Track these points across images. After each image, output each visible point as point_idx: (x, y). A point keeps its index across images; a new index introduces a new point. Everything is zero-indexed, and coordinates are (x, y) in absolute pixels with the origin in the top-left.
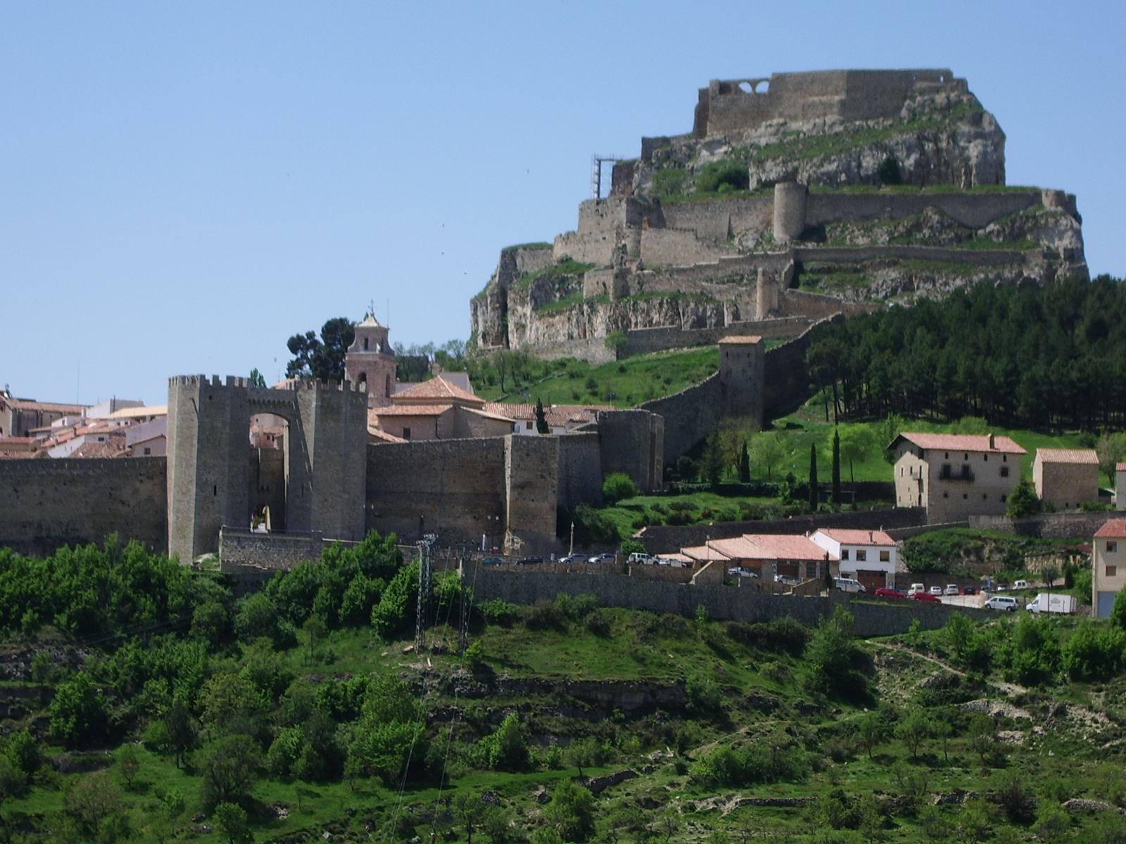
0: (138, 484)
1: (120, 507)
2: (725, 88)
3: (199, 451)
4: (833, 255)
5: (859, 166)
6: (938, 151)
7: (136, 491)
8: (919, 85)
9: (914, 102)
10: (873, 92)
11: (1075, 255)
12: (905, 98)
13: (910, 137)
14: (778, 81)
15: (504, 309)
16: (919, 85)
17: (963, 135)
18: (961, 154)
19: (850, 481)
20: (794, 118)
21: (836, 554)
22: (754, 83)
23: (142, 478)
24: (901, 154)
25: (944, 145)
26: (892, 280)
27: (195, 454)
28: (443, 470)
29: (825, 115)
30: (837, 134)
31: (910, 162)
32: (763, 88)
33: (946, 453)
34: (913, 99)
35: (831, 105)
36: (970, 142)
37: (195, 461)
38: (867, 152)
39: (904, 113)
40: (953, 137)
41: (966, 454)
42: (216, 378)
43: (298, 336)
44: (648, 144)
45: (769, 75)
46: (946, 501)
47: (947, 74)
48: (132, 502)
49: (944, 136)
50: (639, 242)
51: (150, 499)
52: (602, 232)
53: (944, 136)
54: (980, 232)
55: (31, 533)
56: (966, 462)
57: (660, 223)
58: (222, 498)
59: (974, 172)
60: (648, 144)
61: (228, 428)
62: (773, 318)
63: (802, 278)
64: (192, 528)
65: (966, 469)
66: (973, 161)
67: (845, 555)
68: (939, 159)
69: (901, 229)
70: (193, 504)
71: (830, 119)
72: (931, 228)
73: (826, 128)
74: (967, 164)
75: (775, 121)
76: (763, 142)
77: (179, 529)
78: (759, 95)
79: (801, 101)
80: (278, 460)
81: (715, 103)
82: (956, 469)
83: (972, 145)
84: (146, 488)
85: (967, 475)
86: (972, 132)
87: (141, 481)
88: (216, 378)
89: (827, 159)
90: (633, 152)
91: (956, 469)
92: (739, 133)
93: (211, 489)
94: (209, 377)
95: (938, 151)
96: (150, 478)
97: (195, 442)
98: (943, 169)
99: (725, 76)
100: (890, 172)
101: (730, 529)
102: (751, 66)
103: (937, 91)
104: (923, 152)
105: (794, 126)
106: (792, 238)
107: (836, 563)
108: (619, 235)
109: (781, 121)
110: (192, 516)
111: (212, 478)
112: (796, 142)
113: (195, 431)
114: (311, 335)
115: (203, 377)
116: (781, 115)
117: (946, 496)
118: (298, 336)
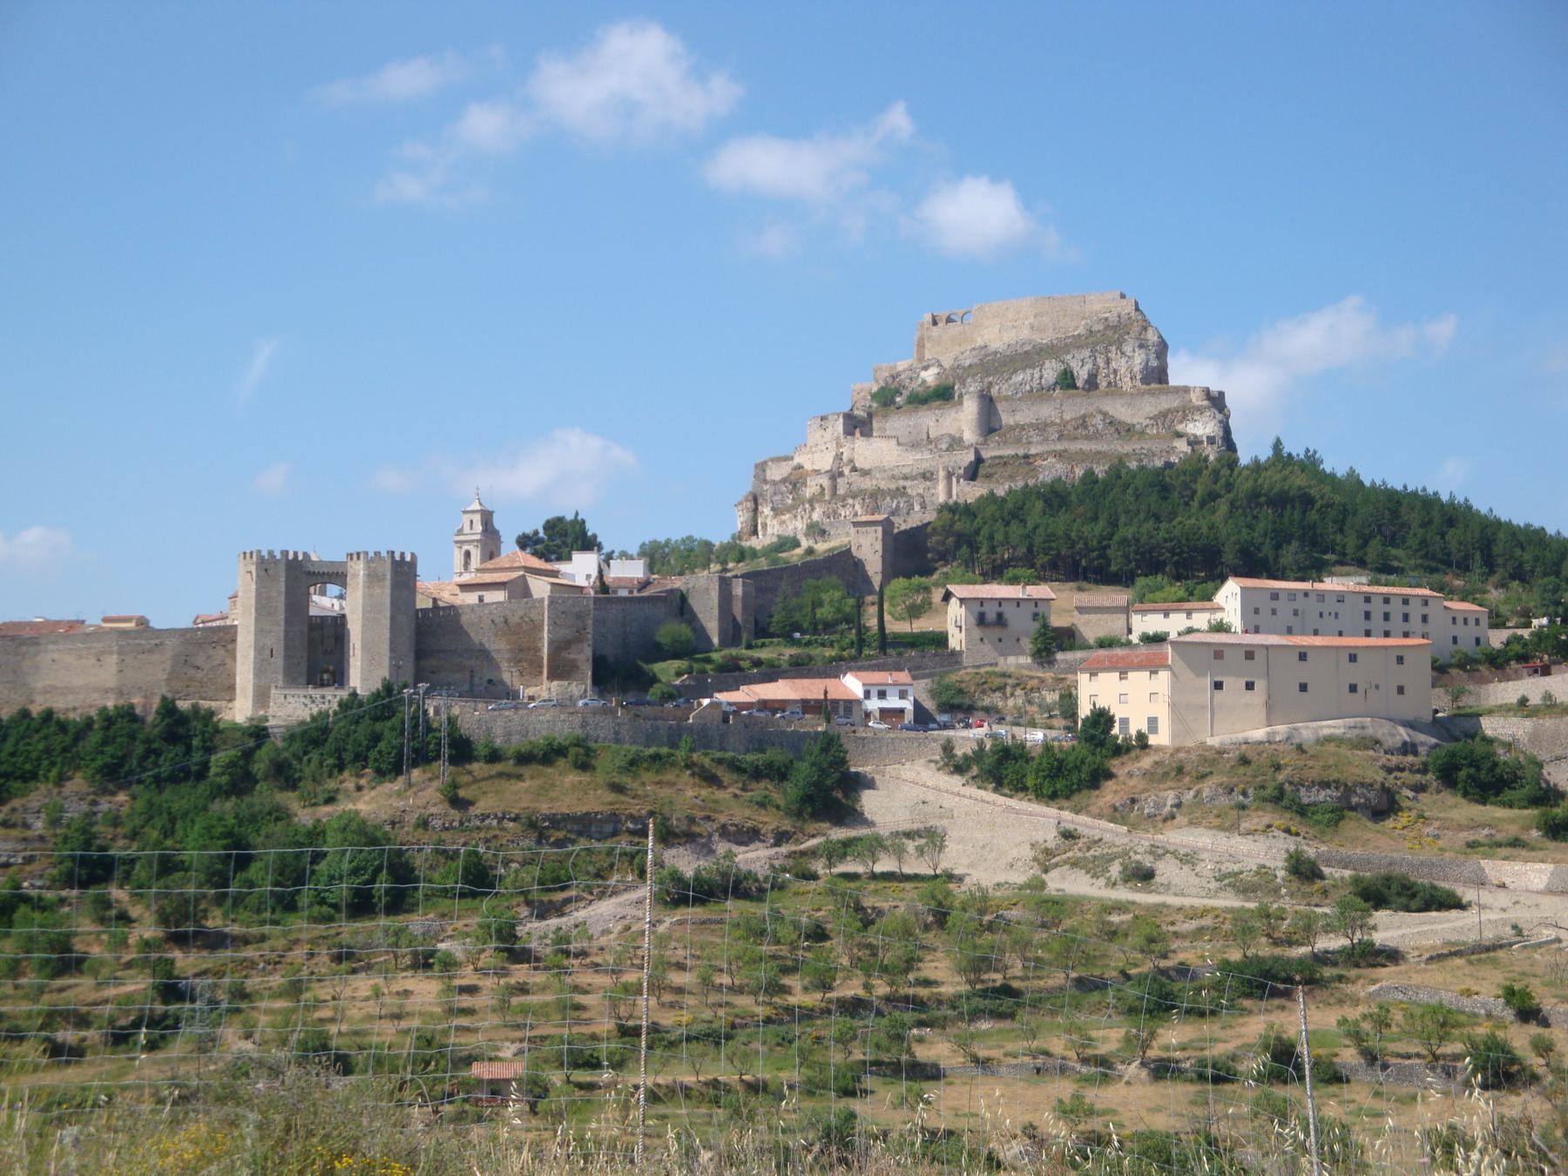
15: (755, 510)
33: (982, 601)
41: (1000, 601)
42: (271, 553)
57: (867, 434)
58: (279, 661)
63: (982, 471)
65: (1000, 615)
67: (867, 695)
76: (967, 363)
82: (991, 616)
85: (1000, 621)
88: (271, 553)
91: (991, 616)
94: (264, 553)
101: (771, 673)
107: (859, 702)
108: (839, 445)
112: (994, 361)
114: (536, 533)
115: (259, 552)
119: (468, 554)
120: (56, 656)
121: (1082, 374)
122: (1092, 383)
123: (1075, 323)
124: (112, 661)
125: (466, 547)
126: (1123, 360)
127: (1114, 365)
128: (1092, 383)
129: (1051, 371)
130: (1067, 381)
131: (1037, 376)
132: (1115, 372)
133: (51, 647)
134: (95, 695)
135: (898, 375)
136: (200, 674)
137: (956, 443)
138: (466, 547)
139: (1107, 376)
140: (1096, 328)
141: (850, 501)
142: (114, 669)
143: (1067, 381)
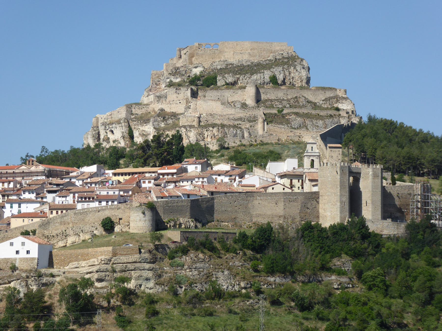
3: (340, 190)
27: (339, 191)
37: (339, 193)
93: (344, 204)
97: (339, 186)
110: (339, 213)
119: (313, 161)
120: (260, 202)
121: (280, 78)
122: (284, 83)
123: (268, 54)
124: (281, 205)
125: (312, 158)
126: (297, 73)
127: (292, 75)
128: (284, 83)
129: (267, 75)
130: (274, 80)
131: (262, 77)
132: (293, 78)
133: (258, 198)
134: (276, 218)
135: (178, 68)
136: (309, 211)
137: (244, 106)
138: (312, 158)
139: (290, 79)
140: (278, 57)
141: (211, 129)
142: (282, 208)
143: (274, 80)
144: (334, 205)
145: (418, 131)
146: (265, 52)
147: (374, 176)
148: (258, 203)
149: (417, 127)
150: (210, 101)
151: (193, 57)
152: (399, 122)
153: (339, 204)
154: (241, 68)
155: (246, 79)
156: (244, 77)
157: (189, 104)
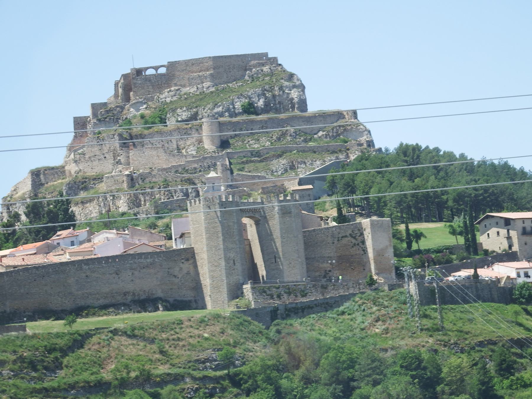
0: (181, 265)
1: (174, 279)
2: (139, 72)
3: (224, 240)
4: (242, 155)
5: (234, 108)
6: (274, 96)
7: (181, 269)
8: (253, 62)
9: (251, 72)
10: (230, 69)
11: (370, 144)
12: (246, 70)
13: (259, 90)
14: (171, 66)
16: (253, 62)
17: (287, 87)
18: (288, 97)
19: (456, 244)
20: (184, 86)
21: (514, 275)
22: (156, 68)
23: (183, 261)
24: (255, 99)
25: (277, 93)
26: (283, 165)
27: (221, 243)
28: (333, 243)
29: (203, 83)
30: (212, 92)
31: (261, 103)
32: (162, 71)
34: (251, 70)
35: (206, 78)
36: (291, 91)
37: (222, 246)
38: (236, 100)
39: (247, 78)
40: (281, 88)
43: (417, 145)
44: (95, 107)
45: (166, 63)
46: (526, 246)
47: (266, 54)
48: (180, 276)
49: (276, 89)
50: (129, 157)
51: (188, 273)
52: (104, 154)
53: (276, 89)
54: (315, 136)
55: (129, 298)
56: (524, 225)
59: (296, 106)
60: (95, 107)
61: (236, 226)
62: (230, 190)
64: (225, 285)
66: (296, 100)
67: (519, 276)
68: (275, 101)
69: (274, 138)
70: (224, 272)
71: (206, 84)
72: (291, 135)
73: (205, 90)
74: (292, 102)
75: (172, 89)
77: (215, 288)
78: (162, 75)
79: (187, 76)
80: (247, 245)
81: (135, 81)
83: (292, 91)
84: (186, 266)
86: (291, 85)
87: (183, 263)
89: (216, 105)
90: (87, 112)
92: (152, 97)
93: (232, 262)
95: (274, 96)
96: (187, 260)
97: (220, 235)
98: (278, 106)
99: (139, 65)
100: (250, 109)
102: (154, 57)
103: (263, 65)
104: (266, 98)
105: (185, 90)
106: (217, 147)
109: (177, 88)
110: (225, 278)
111: (232, 255)
113: (220, 229)
116: (176, 85)
117: (526, 244)
118: (417, 145)
144: (216, 266)
145: (423, 147)
146: (235, 70)
147: (283, 214)
148: (84, 275)
149: (476, 155)
150: (149, 149)
151: (130, 90)
152: (415, 144)
153: (223, 263)
154: (201, 97)
155: (206, 113)
156: (204, 109)
157: (119, 158)
